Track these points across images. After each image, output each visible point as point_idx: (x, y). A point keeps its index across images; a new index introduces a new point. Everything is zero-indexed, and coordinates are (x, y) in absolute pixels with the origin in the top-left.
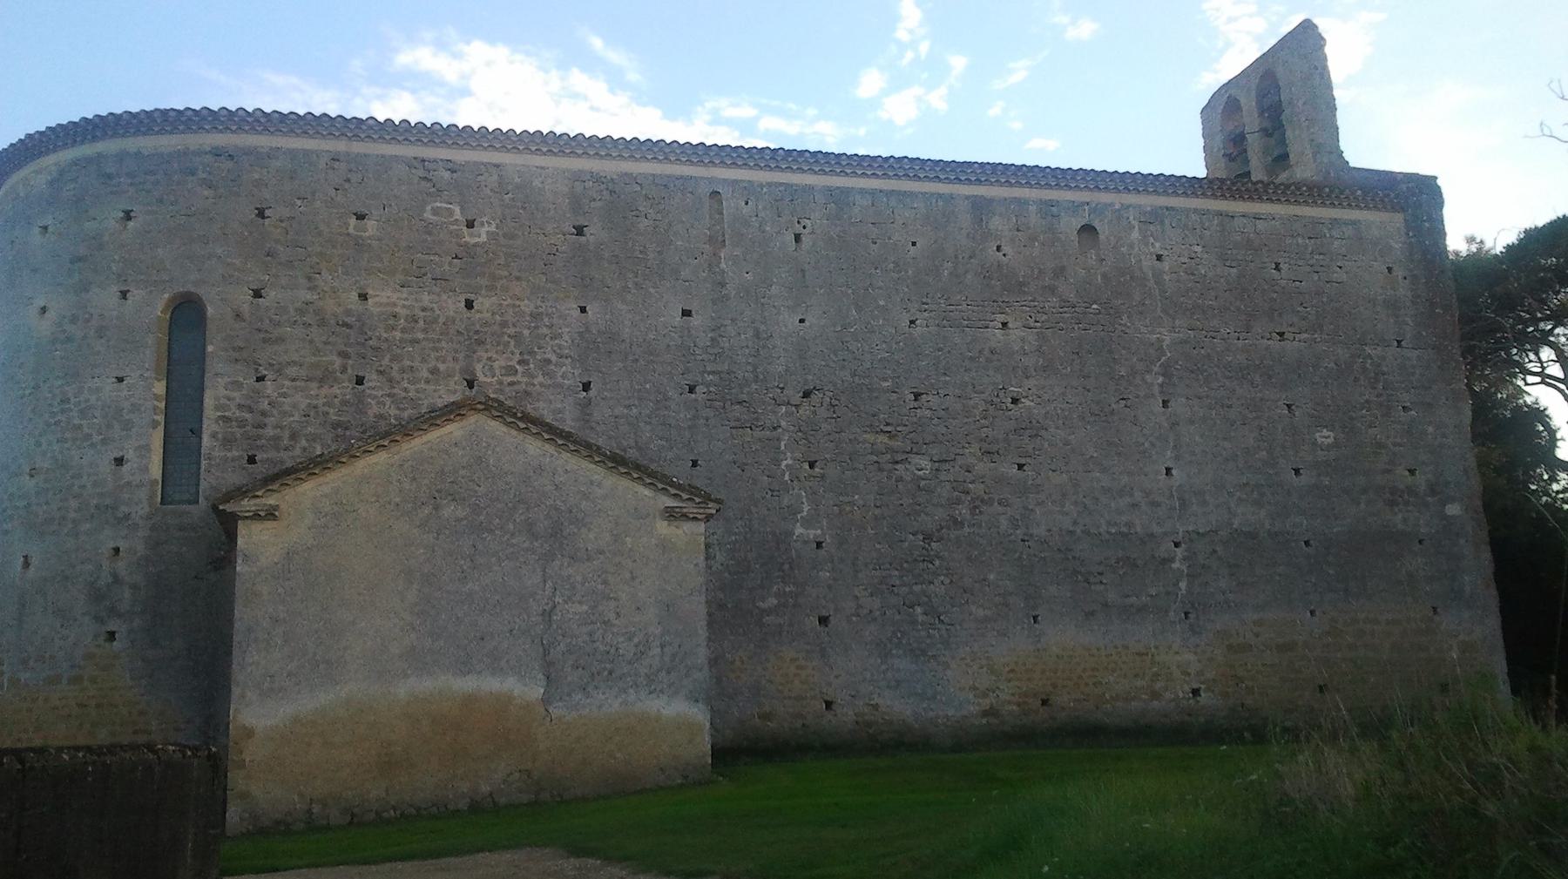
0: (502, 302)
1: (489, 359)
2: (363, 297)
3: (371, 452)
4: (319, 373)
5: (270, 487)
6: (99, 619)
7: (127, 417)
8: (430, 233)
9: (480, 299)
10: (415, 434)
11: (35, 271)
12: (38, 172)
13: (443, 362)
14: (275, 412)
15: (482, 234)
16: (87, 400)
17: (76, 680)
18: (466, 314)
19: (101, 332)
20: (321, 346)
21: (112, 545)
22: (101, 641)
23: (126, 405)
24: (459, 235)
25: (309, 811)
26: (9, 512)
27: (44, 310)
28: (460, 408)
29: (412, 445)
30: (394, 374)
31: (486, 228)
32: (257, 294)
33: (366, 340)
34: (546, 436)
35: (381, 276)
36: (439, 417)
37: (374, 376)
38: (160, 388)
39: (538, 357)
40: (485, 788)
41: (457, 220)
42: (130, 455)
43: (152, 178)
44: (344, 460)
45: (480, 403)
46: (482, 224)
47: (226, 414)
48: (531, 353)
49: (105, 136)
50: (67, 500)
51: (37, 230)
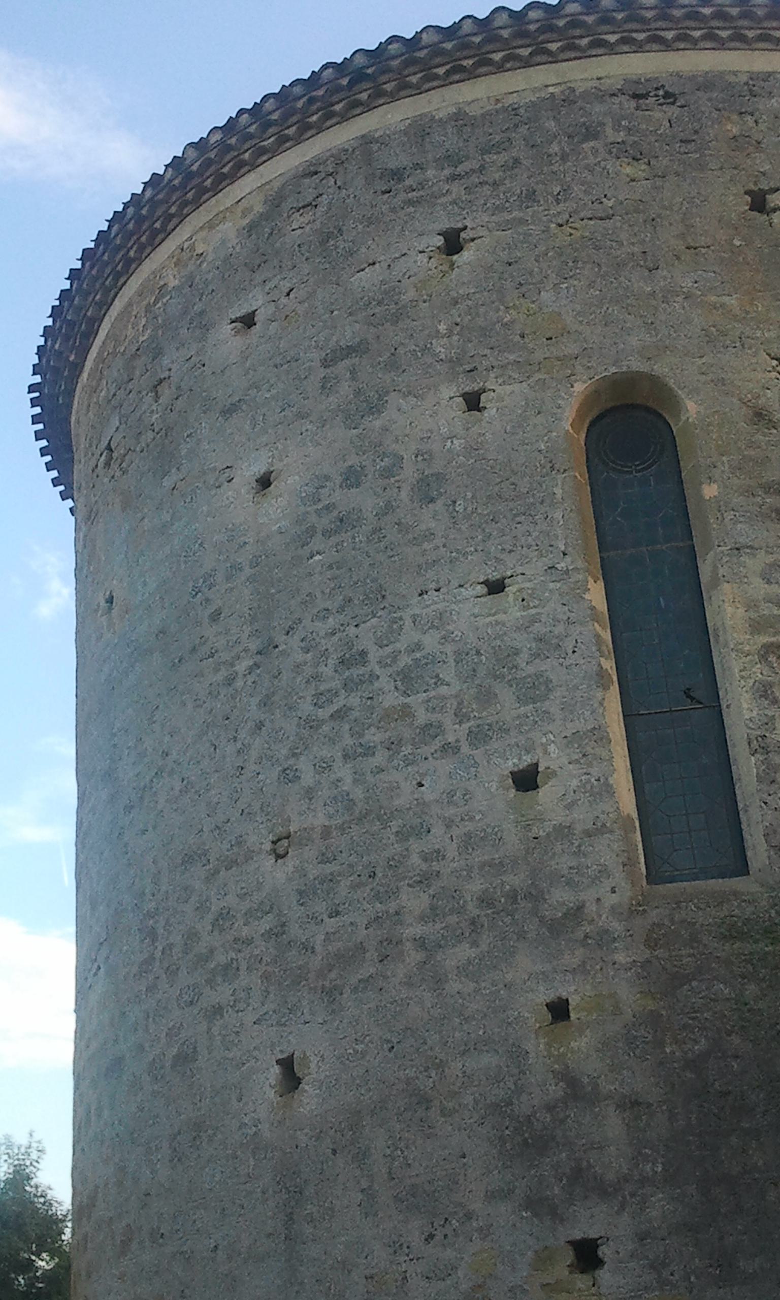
7: (531, 670)
11: (229, 411)
16: (418, 646)
21: (544, 995)
22: (561, 1269)
23: (524, 642)
26: (221, 958)
27: (265, 482)
38: (596, 594)
43: (503, 158)
49: (380, 96)
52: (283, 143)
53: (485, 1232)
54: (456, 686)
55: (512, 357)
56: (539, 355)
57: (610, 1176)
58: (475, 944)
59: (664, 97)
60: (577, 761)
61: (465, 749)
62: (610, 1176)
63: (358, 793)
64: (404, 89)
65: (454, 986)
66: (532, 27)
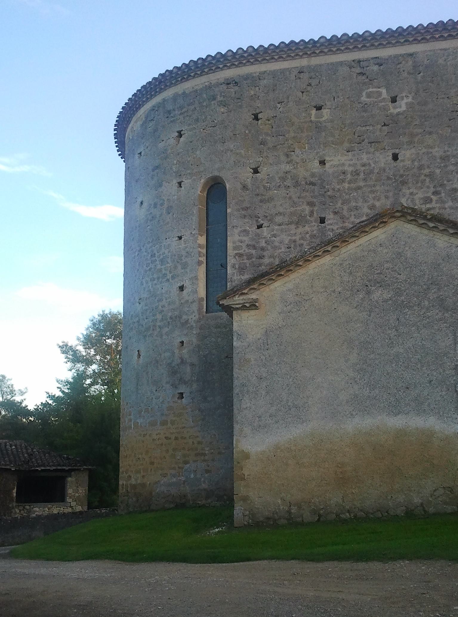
0: (419, 151)
1: (411, 194)
2: (322, 163)
3: (319, 256)
4: (295, 218)
5: (252, 287)
6: (174, 386)
8: (365, 111)
9: (403, 152)
10: (350, 241)
12: (136, 122)
13: (378, 200)
14: (269, 247)
15: (402, 106)
17: (164, 423)
18: (394, 164)
19: (169, 210)
20: (296, 200)
23: (184, 253)
24: (385, 109)
25: (289, 512)
28: (382, 216)
29: (348, 249)
30: (345, 213)
31: (405, 100)
32: (256, 171)
33: (325, 192)
34: (451, 231)
35: (334, 146)
36: (366, 225)
37: (332, 216)
38: (202, 240)
39: (448, 188)
40: (417, 500)
41: (384, 99)
42: (187, 284)
44: (301, 263)
45: (397, 211)
46: (402, 99)
47: (240, 252)
48: (442, 185)
49: (166, 87)
50: (156, 315)
51: (137, 156)
52: (148, 100)
53: (165, 390)
54: (171, 264)
55: (189, 171)
56: (195, 171)
57: (187, 380)
58: (168, 328)
59: (235, 83)
60: (191, 284)
61: (171, 280)
62: (187, 380)
63: (152, 290)
64: (171, 85)
65: (164, 337)
66: (199, 66)
